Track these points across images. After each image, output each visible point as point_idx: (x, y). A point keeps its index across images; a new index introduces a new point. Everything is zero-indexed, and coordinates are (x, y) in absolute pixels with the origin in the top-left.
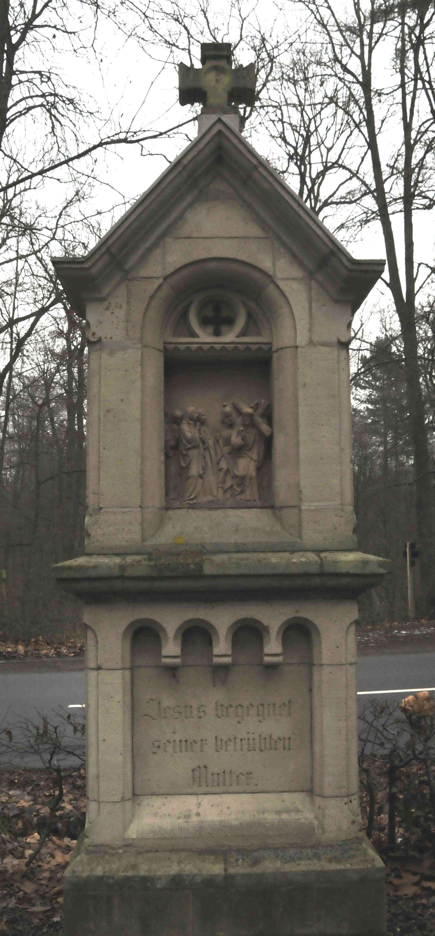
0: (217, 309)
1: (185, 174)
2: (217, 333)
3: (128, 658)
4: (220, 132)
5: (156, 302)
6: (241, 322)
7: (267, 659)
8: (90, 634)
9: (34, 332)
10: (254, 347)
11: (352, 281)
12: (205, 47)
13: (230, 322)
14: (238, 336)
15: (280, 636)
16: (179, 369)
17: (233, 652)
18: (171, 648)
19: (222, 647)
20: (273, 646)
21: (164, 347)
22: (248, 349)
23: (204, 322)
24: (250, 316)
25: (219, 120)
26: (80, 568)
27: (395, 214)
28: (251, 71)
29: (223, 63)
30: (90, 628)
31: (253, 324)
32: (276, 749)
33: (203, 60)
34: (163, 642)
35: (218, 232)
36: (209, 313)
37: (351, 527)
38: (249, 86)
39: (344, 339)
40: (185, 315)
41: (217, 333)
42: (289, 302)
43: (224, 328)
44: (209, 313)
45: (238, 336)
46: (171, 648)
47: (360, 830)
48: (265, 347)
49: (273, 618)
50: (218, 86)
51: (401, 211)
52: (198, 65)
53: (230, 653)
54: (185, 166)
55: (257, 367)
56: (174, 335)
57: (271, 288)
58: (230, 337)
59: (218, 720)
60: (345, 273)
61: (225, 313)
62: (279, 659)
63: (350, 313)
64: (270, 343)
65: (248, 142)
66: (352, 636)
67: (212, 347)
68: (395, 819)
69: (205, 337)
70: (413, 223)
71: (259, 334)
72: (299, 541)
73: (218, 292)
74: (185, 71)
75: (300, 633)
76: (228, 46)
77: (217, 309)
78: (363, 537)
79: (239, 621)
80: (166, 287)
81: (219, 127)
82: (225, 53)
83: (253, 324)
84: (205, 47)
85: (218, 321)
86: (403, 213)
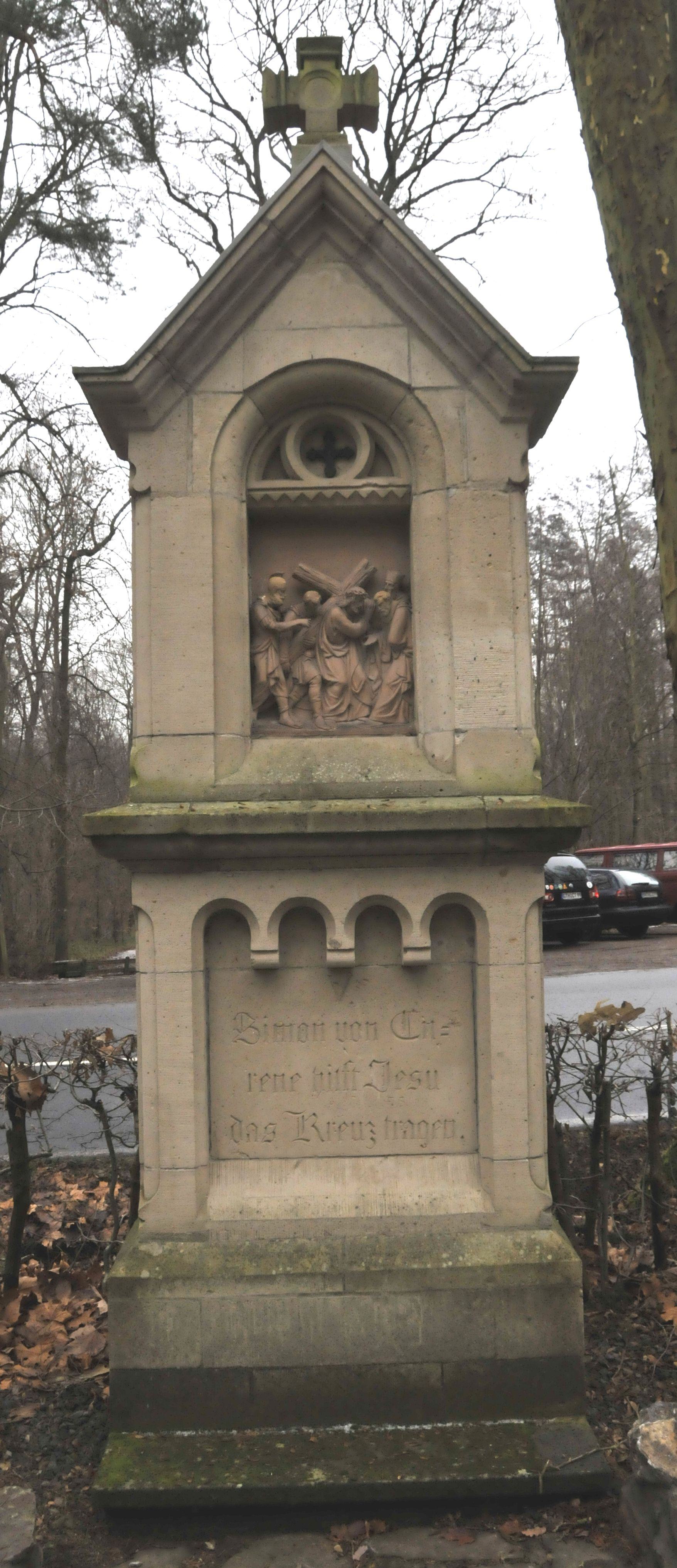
1: (272, 236)
2: (331, 473)
3: (201, 958)
4: (323, 170)
5: (229, 430)
7: (409, 957)
8: (142, 922)
10: (365, 491)
12: (303, 43)
13: (350, 455)
15: (428, 923)
16: (269, 525)
18: (264, 940)
19: (416, 935)
20: (416, 935)
22: (356, 495)
23: (310, 457)
25: (322, 151)
29: (328, 66)
30: (145, 913)
31: (380, 461)
33: (300, 65)
34: (253, 932)
35: (324, 324)
36: (318, 444)
37: (528, 760)
38: (370, 103)
39: (518, 478)
41: (331, 473)
43: (340, 465)
44: (318, 444)
45: (359, 477)
46: (264, 940)
47: (547, 1210)
48: (400, 492)
49: (415, 898)
50: (323, 102)
52: (293, 71)
53: (428, 944)
54: (273, 223)
55: (390, 522)
56: (265, 477)
57: (410, 403)
58: (350, 479)
59: (333, 1052)
60: (515, 375)
61: (341, 445)
62: (426, 956)
64: (409, 486)
66: (535, 919)
69: (311, 479)
71: (391, 473)
72: (451, 778)
73: (324, 412)
75: (455, 918)
76: (338, 42)
78: (548, 788)
80: (249, 408)
81: (322, 161)
82: (357, 86)
83: (380, 461)
84: (303, 43)
85: (328, 451)
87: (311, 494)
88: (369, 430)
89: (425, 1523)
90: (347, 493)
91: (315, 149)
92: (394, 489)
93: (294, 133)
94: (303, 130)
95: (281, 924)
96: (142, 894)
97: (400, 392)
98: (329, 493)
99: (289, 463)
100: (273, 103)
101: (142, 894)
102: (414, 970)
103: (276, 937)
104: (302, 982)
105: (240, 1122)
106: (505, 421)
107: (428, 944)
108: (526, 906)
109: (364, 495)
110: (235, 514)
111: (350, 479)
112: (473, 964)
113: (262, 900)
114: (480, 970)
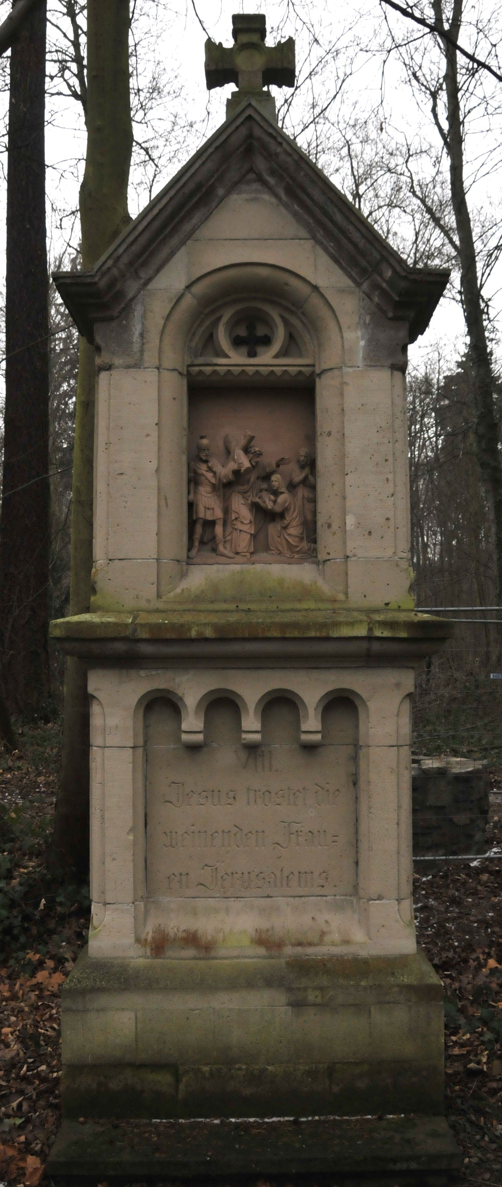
0: (251, 328)
4: (250, 118)
6: (276, 347)
9: (447, 241)
11: (406, 298)
13: (267, 341)
14: (276, 356)
15: (320, 710)
16: (203, 392)
17: (263, 725)
18: (192, 723)
19: (311, 723)
21: (188, 371)
23: (237, 342)
24: (291, 338)
25: (250, 105)
26: (91, 625)
27: (61, 96)
28: (288, 47)
29: (255, 38)
32: (314, 366)
35: (249, 235)
36: (242, 332)
38: (285, 65)
40: (210, 339)
41: (252, 354)
42: (336, 316)
43: (260, 349)
45: (276, 356)
46: (192, 723)
49: (311, 690)
51: (50, 11)
53: (259, 729)
55: (299, 393)
58: (267, 359)
61: (261, 331)
63: (403, 333)
65: (285, 133)
66: (407, 707)
67: (243, 371)
68: (482, 324)
70: (4, 257)
71: (301, 355)
73: (252, 305)
74: (211, 47)
75: (342, 704)
77: (251, 328)
79: (269, 693)
82: (257, 26)
84: (237, 19)
85: (251, 341)
86: (48, 9)
87: (236, 370)
88: (282, 317)
89: (365, 962)
90: (264, 370)
91: (244, 104)
92: (302, 369)
93: (231, 88)
94: (237, 86)
95: (323, 711)
96: (99, 683)
97: (305, 290)
98: (250, 370)
99: (218, 338)
100: (213, 68)
101: (99, 683)
102: (310, 748)
103: (260, 725)
104: (226, 756)
105: (241, 830)
106: (394, 319)
107: (259, 729)
108: (400, 698)
109: (279, 374)
110: (175, 387)
111: (267, 359)
112: (356, 746)
113: (192, 690)
114: (362, 752)
